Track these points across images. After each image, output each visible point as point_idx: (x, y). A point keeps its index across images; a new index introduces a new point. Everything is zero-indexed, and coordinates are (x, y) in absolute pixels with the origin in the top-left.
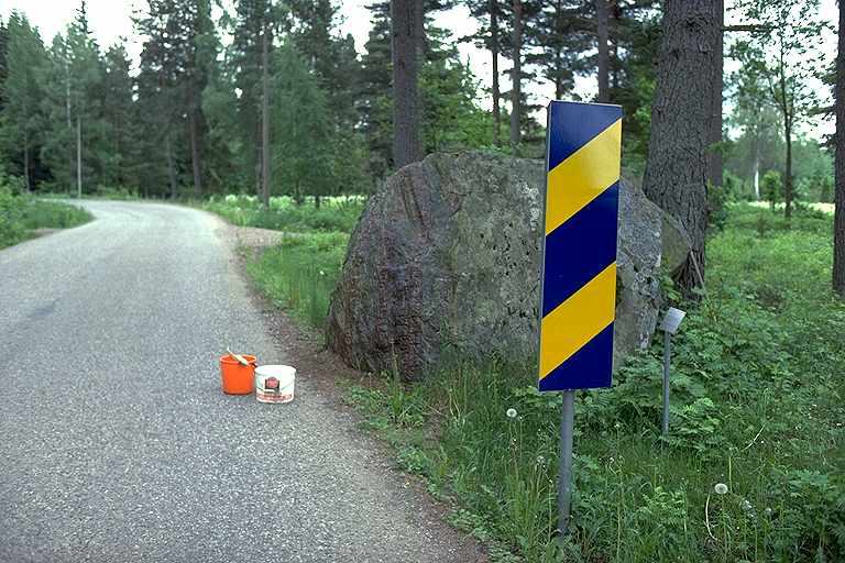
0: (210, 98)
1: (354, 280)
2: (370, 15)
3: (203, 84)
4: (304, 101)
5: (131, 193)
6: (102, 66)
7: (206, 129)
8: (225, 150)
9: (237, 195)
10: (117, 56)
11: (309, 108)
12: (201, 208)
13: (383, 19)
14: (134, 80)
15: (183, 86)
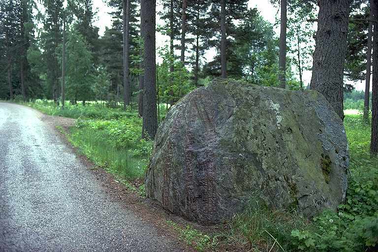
0: (30, 53)
1: (169, 157)
2: (110, 17)
4: (81, 55)
9: (42, 99)
11: (83, 59)
12: (27, 106)
13: (116, 19)
15: (17, 46)
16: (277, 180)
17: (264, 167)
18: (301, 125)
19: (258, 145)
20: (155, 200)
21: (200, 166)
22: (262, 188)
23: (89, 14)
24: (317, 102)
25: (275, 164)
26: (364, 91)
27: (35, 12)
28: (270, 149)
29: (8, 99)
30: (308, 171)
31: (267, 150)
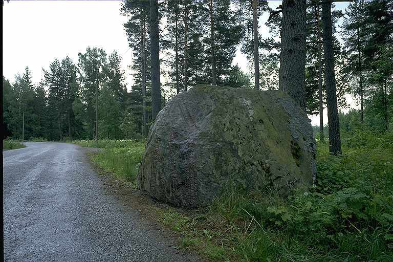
3: (72, 100)
5: (44, 139)
6: (35, 95)
7: (74, 116)
8: (81, 124)
10: (40, 91)
11: (113, 107)
14: (47, 99)
16: (252, 165)
17: (240, 154)
18: (271, 117)
19: (234, 136)
20: (145, 191)
21: (183, 156)
22: (239, 172)
23: (118, 76)
24: (284, 99)
25: (250, 151)
26: (319, 125)
27: (78, 76)
28: (244, 138)
29: (58, 140)
30: (280, 156)
31: (242, 139)
